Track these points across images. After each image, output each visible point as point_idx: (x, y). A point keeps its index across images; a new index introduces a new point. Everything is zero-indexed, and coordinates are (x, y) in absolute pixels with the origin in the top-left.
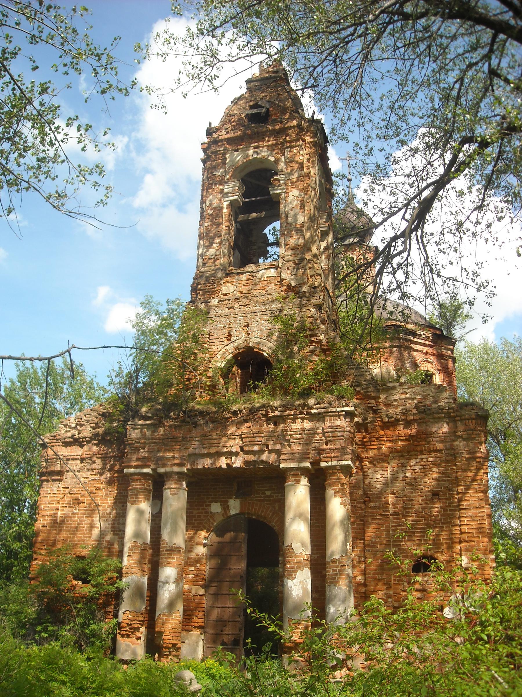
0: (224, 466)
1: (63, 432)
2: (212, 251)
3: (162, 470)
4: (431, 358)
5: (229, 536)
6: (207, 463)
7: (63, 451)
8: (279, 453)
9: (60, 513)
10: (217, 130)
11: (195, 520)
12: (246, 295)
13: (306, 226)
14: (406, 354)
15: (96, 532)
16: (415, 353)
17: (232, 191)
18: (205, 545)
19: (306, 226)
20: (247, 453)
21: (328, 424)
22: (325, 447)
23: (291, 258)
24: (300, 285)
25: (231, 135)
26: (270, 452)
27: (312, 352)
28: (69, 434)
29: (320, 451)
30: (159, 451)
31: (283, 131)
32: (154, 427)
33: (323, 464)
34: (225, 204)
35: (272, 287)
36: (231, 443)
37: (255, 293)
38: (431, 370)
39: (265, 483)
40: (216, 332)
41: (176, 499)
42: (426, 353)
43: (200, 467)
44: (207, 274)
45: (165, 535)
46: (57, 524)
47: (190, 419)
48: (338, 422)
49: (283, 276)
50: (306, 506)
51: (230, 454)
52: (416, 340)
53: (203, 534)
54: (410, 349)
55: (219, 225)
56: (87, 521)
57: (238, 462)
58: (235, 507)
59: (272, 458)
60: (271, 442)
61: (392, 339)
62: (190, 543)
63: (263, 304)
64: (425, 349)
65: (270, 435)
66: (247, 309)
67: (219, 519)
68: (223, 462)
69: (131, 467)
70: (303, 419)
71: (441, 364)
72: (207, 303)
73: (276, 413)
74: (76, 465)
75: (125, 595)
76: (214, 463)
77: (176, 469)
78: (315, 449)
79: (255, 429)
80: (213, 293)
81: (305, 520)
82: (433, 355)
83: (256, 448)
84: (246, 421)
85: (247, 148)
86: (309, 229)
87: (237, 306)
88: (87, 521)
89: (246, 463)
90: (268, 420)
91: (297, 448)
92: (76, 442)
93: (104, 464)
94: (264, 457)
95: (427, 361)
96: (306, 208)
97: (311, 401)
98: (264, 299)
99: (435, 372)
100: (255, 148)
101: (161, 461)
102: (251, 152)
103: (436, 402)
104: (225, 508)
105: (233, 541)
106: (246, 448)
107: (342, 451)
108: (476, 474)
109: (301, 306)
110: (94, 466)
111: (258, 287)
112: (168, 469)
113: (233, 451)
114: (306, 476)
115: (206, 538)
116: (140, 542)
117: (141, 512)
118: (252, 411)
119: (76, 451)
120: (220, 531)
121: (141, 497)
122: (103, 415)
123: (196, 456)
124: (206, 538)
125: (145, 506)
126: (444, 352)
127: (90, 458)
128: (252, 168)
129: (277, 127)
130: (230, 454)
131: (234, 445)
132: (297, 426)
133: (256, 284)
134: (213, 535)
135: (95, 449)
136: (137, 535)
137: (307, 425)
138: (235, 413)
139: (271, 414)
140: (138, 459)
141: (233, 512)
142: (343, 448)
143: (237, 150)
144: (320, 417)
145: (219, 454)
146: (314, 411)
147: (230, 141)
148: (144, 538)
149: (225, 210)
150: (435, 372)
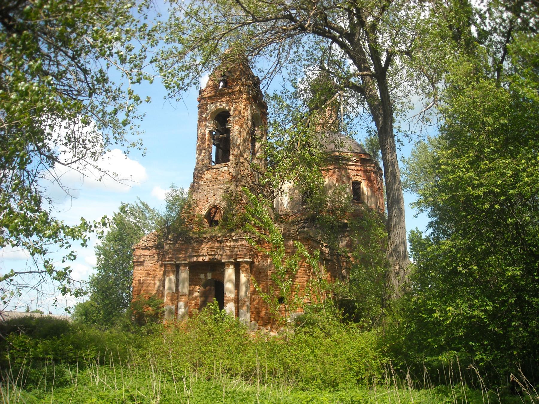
0: (201, 261)
1: (142, 244)
2: (201, 158)
3: (178, 262)
4: (360, 173)
5: (208, 288)
6: (195, 259)
7: (143, 252)
8: (222, 255)
9: (142, 279)
10: (203, 91)
11: (193, 281)
12: (215, 180)
13: (241, 144)
14: (343, 173)
15: (156, 287)
16: (349, 171)
17: (210, 125)
18: (198, 292)
19: (241, 144)
20: (210, 255)
21: (240, 243)
22: (239, 253)
23: (234, 162)
24: (237, 175)
25: (209, 95)
26: (218, 255)
27: (240, 208)
28: (144, 245)
29: (237, 255)
30: (177, 254)
31: (233, 93)
32: (174, 244)
33: (238, 260)
34: (207, 132)
35: (226, 175)
36: (203, 251)
37: (219, 178)
38: (360, 180)
39: (216, 267)
40: (202, 198)
41: (184, 274)
42: (357, 170)
43: (192, 261)
44: (199, 169)
45: (180, 290)
46: (141, 283)
47: (188, 241)
48: (243, 243)
49: (230, 171)
50: (233, 277)
51: (203, 256)
52: (350, 163)
53: (198, 287)
54: (346, 169)
55: (204, 143)
56: (153, 282)
57: (206, 259)
58: (209, 276)
59: (219, 257)
60: (218, 251)
61: (335, 164)
62: (191, 292)
63: (221, 184)
64: (356, 168)
65: (218, 248)
66: (215, 187)
67: (204, 281)
68: (201, 259)
69: (166, 261)
70: (230, 241)
71: (367, 175)
72: (198, 183)
73: (220, 239)
74: (148, 258)
75: (165, 313)
76: (197, 259)
77: (183, 262)
78: (235, 254)
79: (212, 245)
80: (201, 178)
81: (232, 282)
82: (361, 170)
83: (213, 253)
84: (209, 242)
85: (216, 102)
86: (243, 145)
87: (211, 185)
88: (153, 282)
89: (210, 259)
90: (218, 241)
91: (228, 253)
92: (146, 248)
93: (159, 258)
94: (216, 257)
95: (357, 175)
96: (242, 135)
97: (233, 234)
98: (222, 182)
99: (362, 181)
100: (220, 102)
101: (178, 259)
102: (218, 104)
103: (289, 231)
104: (206, 276)
105: (210, 289)
106: (209, 253)
107: (245, 255)
108: (302, 263)
109: (237, 186)
110: (154, 258)
111: (220, 176)
112: (180, 262)
113: (204, 254)
114: (232, 265)
115: (199, 289)
116: (171, 292)
117: (170, 280)
118: (211, 237)
119: (147, 252)
120: (204, 286)
121: (171, 273)
122: (157, 236)
123: (190, 257)
124: (199, 289)
125: (173, 277)
126: (369, 168)
127: (153, 255)
128: (217, 114)
129: (230, 91)
130: (203, 256)
131: (204, 252)
132: (228, 244)
133: (219, 174)
134: (202, 288)
135: (154, 251)
136: (170, 288)
137: (232, 243)
138: (205, 238)
139: (218, 239)
140: (169, 258)
141: (209, 278)
142: (245, 254)
143: (212, 103)
144: (236, 241)
145: (199, 256)
146: (234, 238)
147: (210, 98)
148: (172, 290)
149: (207, 136)
150: (362, 181)
